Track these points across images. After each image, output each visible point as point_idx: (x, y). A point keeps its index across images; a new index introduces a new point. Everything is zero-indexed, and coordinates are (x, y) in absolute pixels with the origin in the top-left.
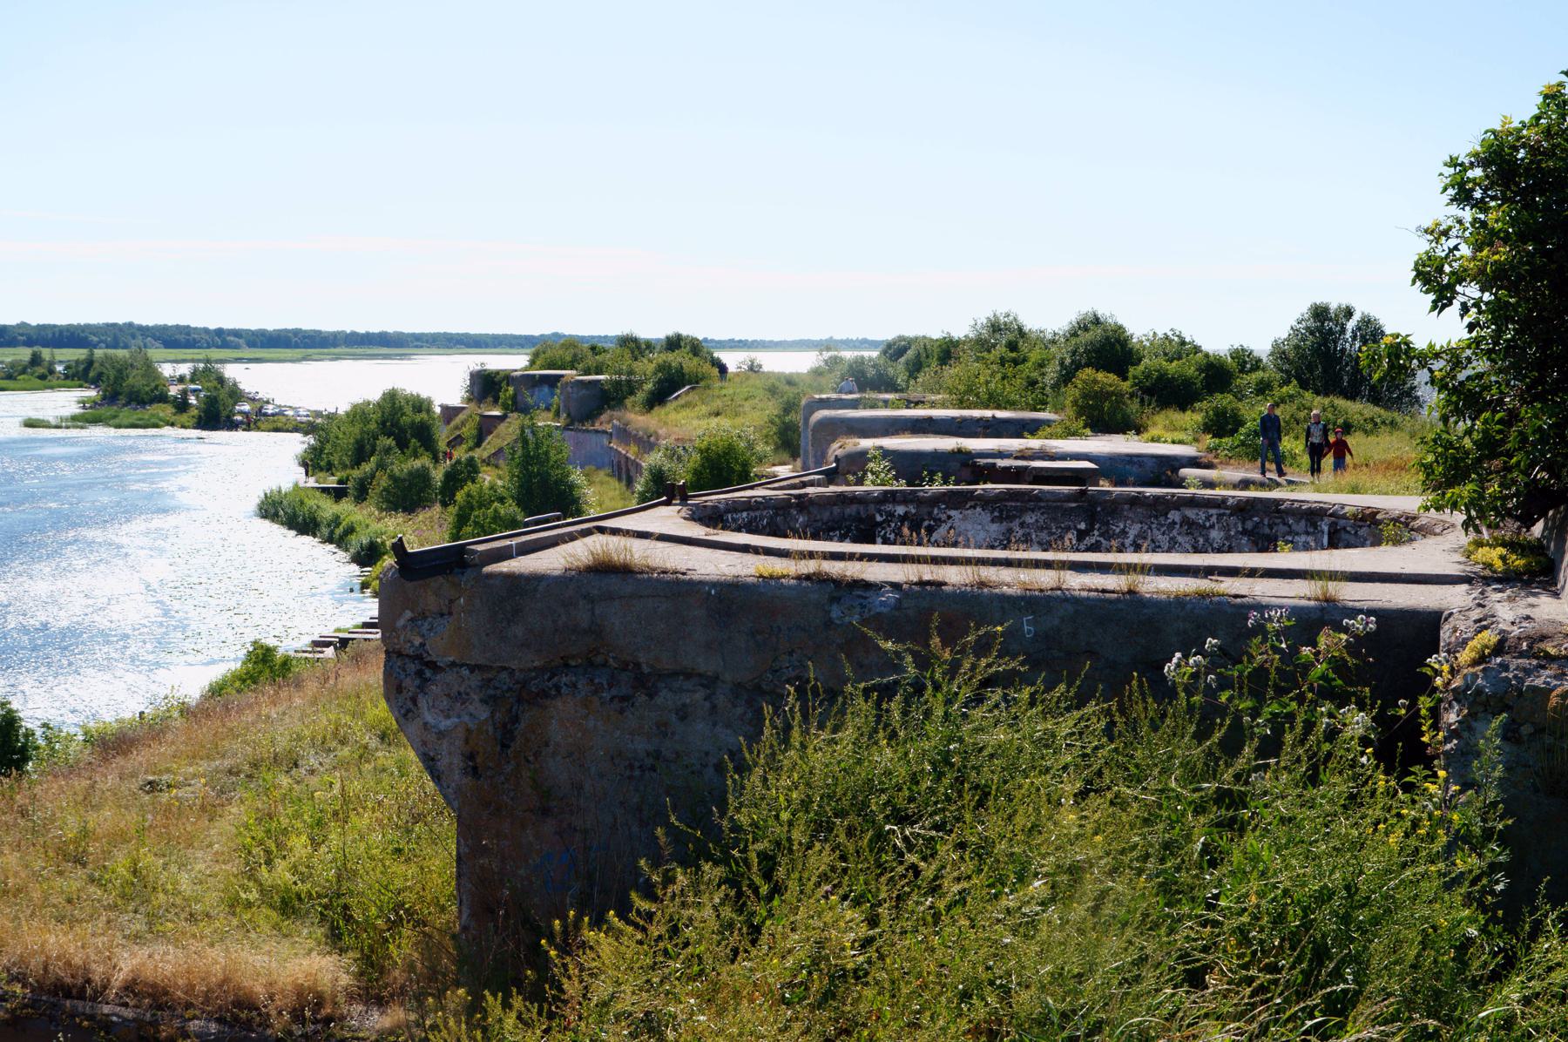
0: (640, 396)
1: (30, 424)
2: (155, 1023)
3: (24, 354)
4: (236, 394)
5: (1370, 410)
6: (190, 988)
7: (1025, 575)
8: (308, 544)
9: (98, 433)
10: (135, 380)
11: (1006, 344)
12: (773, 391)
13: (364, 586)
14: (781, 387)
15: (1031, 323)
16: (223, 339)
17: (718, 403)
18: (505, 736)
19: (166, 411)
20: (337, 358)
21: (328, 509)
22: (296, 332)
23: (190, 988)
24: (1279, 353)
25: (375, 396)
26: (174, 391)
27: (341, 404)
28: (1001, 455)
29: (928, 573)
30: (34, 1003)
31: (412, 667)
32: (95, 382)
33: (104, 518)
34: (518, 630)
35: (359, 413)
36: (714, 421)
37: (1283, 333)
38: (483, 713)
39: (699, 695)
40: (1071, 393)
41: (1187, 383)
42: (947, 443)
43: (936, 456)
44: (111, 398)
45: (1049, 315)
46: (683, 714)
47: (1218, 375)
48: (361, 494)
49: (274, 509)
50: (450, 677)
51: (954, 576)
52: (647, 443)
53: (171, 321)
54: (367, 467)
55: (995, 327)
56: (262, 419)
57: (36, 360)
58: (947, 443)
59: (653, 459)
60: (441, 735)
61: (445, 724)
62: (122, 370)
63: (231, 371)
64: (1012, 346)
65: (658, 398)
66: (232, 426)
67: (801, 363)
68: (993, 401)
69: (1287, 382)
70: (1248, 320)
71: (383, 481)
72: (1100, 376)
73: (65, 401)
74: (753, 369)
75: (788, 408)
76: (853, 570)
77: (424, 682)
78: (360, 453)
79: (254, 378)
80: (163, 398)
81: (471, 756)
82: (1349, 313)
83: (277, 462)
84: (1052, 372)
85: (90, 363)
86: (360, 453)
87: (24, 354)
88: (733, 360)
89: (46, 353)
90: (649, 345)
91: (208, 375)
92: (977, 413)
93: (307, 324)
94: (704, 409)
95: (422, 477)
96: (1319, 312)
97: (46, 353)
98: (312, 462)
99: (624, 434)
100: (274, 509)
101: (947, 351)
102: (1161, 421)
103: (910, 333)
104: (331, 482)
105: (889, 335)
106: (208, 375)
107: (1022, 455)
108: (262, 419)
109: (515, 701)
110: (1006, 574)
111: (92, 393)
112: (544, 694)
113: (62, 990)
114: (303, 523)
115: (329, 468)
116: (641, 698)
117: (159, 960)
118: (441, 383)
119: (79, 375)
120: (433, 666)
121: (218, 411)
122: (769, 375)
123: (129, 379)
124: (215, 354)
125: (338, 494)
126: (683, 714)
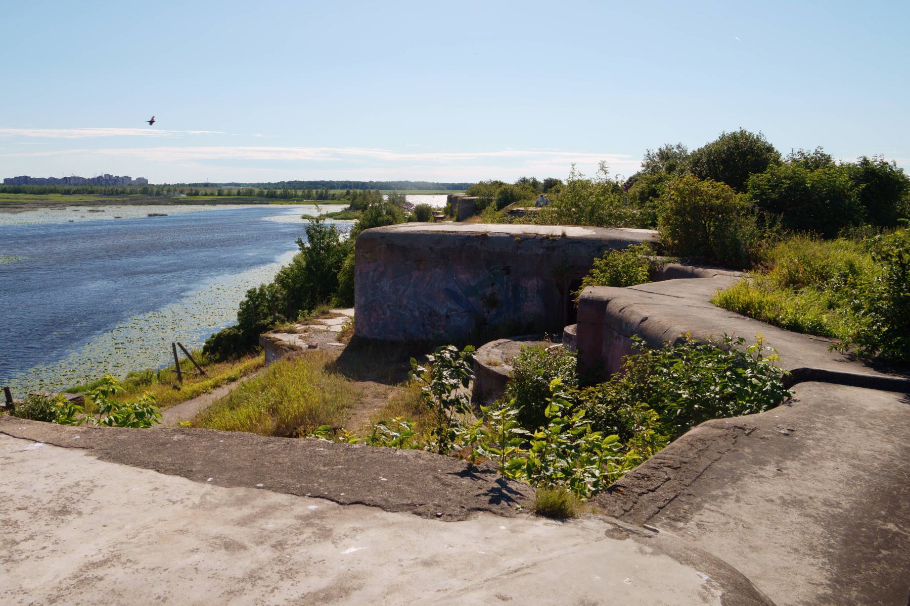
1: (150, 215)
57: (348, 193)
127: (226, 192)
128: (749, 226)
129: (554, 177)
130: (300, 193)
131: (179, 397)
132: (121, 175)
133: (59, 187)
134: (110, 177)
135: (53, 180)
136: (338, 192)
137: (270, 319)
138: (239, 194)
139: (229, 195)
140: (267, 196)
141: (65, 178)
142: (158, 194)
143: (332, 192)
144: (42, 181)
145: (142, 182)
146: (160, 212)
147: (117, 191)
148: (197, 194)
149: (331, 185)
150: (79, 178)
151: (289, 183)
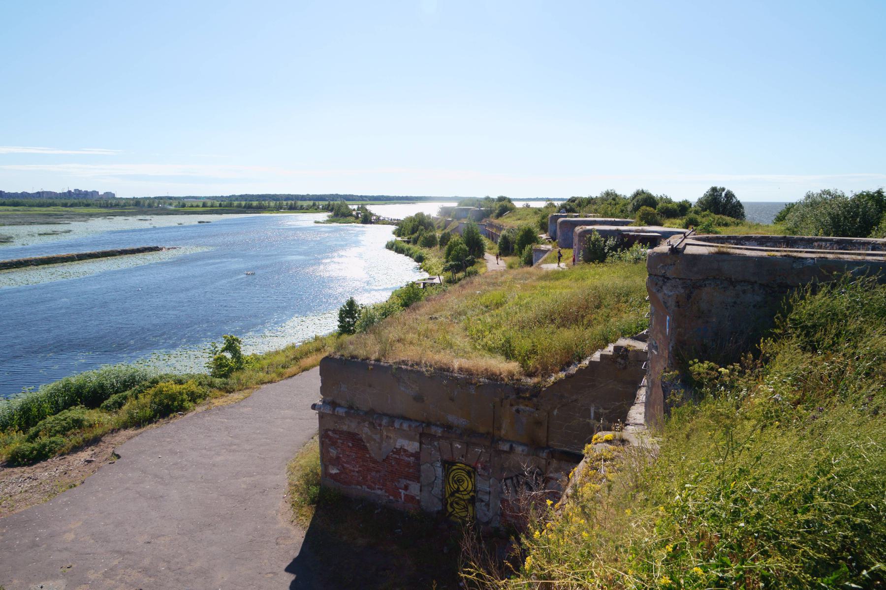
0: (494, 214)
1: (316, 222)
2: (471, 379)
3: (311, 203)
4: (372, 214)
5: (733, 219)
6: (477, 371)
7: (853, 256)
8: (401, 256)
9: (335, 224)
10: (343, 210)
11: (611, 198)
12: (536, 213)
13: (421, 268)
14: (537, 211)
15: (619, 192)
16: (362, 198)
17: (519, 217)
18: (689, 297)
19: (353, 219)
20: (395, 203)
21: (406, 246)
22: (383, 196)
23: (477, 371)
24: (700, 202)
25: (413, 215)
26: (354, 213)
27: (402, 218)
28: (630, 231)
29: (822, 255)
30: (435, 372)
31: (661, 279)
32: (331, 211)
33: (343, 247)
34: (695, 269)
35: (411, 219)
36: (519, 222)
37: (702, 195)
38: (682, 291)
39: (749, 287)
40: (639, 213)
41: (675, 210)
42: (614, 228)
43: (610, 231)
44: (336, 215)
45: (626, 191)
46: (744, 292)
47: (683, 209)
48: (415, 242)
49: (390, 246)
50: (673, 281)
51: (830, 256)
52: (500, 228)
53: (348, 193)
54: (416, 235)
55: (608, 194)
56: (379, 221)
57: (314, 205)
58: (614, 228)
59: (504, 232)
60: (669, 296)
61: (670, 294)
62: (340, 207)
63: (368, 207)
64: (614, 199)
65: (500, 215)
66: (371, 223)
67: (542, 205)
68: (612, 216)
69: (705, 210)
70: (692, 192)
71: (422, 238)
72: (648, 208)
73: (323, 216)
74: (528, 206)
75: (544, 217)
76: (800, 255)
77: (664, 283)
78: (414, 231)
79: (375, 209)
80: (351, 215)
81: (678, 302)
82: (723, 189)
83: (387, 233)
84: (630, 207)
85: (329, 205)
86: (414, 231)
87: (311, 203)
88: (518, 205)
89: (317, 203)
90: (493, 200)
91: (362, 208)
92: (609, 219)
93: (386, 194)
94: (515, 218)
95: (434, 237)
96: (714, 189)
97: (317, 203)
98: (398, 233)
99: (491, 225)
100: (390, 246)
101: (590, 201)
102: (667, 222)
103: (576, 196)
104: (406, 239)
105: (569, 197)
106: (362, 208)
107: (636, 231)
108: (379, 221)
109: (692, 288)
110: (845, 256)
111: (330, 214)
112: (701, 286)
113: (442, 369)
114: (399, 251)
115: (404, 234)
116: (731, 287)
117: (465, 363)
118: (431, 210)
119: (326, 209)
120: (668, 279)
121: (367, 219)
122: (533, 208)
123: (342, 210)
124: (364, 202)
125: (408, 242)
126: (744, 292)
127: (209, 204)
128: (659, 218)
129: (504, 195)
130: (272, 204)
131: (644, 207)
132: (90, 190)
133: (57, 201)
134: (80, 191)
135: (24, 195)
136: (305, 204)
137: (683, 495)
138: (220, 205)
139: (212, 206)
140: (245, 207)
141: (38, 193)
142: (150, 206)
143: (300, 203)
144: (16, 195)
145: (110, 195)
146: (45, 238)
147: (111, 204)
148: (184, 206)
149: (303, 198)
150: (51, 193)
151: (241, 196)
